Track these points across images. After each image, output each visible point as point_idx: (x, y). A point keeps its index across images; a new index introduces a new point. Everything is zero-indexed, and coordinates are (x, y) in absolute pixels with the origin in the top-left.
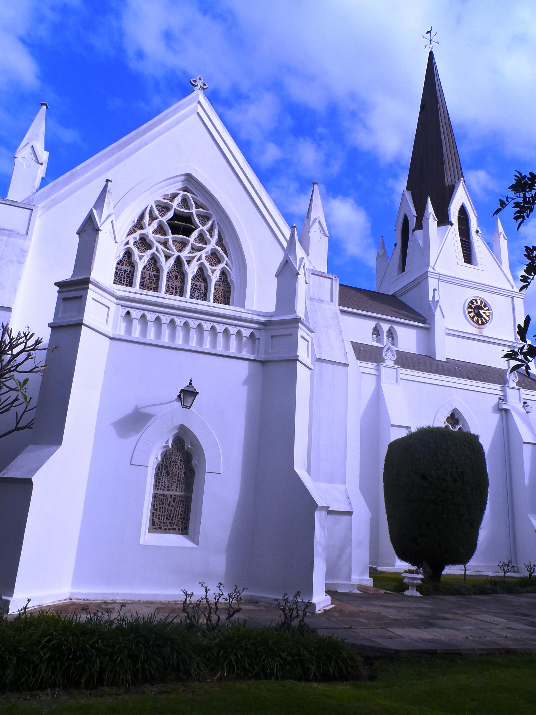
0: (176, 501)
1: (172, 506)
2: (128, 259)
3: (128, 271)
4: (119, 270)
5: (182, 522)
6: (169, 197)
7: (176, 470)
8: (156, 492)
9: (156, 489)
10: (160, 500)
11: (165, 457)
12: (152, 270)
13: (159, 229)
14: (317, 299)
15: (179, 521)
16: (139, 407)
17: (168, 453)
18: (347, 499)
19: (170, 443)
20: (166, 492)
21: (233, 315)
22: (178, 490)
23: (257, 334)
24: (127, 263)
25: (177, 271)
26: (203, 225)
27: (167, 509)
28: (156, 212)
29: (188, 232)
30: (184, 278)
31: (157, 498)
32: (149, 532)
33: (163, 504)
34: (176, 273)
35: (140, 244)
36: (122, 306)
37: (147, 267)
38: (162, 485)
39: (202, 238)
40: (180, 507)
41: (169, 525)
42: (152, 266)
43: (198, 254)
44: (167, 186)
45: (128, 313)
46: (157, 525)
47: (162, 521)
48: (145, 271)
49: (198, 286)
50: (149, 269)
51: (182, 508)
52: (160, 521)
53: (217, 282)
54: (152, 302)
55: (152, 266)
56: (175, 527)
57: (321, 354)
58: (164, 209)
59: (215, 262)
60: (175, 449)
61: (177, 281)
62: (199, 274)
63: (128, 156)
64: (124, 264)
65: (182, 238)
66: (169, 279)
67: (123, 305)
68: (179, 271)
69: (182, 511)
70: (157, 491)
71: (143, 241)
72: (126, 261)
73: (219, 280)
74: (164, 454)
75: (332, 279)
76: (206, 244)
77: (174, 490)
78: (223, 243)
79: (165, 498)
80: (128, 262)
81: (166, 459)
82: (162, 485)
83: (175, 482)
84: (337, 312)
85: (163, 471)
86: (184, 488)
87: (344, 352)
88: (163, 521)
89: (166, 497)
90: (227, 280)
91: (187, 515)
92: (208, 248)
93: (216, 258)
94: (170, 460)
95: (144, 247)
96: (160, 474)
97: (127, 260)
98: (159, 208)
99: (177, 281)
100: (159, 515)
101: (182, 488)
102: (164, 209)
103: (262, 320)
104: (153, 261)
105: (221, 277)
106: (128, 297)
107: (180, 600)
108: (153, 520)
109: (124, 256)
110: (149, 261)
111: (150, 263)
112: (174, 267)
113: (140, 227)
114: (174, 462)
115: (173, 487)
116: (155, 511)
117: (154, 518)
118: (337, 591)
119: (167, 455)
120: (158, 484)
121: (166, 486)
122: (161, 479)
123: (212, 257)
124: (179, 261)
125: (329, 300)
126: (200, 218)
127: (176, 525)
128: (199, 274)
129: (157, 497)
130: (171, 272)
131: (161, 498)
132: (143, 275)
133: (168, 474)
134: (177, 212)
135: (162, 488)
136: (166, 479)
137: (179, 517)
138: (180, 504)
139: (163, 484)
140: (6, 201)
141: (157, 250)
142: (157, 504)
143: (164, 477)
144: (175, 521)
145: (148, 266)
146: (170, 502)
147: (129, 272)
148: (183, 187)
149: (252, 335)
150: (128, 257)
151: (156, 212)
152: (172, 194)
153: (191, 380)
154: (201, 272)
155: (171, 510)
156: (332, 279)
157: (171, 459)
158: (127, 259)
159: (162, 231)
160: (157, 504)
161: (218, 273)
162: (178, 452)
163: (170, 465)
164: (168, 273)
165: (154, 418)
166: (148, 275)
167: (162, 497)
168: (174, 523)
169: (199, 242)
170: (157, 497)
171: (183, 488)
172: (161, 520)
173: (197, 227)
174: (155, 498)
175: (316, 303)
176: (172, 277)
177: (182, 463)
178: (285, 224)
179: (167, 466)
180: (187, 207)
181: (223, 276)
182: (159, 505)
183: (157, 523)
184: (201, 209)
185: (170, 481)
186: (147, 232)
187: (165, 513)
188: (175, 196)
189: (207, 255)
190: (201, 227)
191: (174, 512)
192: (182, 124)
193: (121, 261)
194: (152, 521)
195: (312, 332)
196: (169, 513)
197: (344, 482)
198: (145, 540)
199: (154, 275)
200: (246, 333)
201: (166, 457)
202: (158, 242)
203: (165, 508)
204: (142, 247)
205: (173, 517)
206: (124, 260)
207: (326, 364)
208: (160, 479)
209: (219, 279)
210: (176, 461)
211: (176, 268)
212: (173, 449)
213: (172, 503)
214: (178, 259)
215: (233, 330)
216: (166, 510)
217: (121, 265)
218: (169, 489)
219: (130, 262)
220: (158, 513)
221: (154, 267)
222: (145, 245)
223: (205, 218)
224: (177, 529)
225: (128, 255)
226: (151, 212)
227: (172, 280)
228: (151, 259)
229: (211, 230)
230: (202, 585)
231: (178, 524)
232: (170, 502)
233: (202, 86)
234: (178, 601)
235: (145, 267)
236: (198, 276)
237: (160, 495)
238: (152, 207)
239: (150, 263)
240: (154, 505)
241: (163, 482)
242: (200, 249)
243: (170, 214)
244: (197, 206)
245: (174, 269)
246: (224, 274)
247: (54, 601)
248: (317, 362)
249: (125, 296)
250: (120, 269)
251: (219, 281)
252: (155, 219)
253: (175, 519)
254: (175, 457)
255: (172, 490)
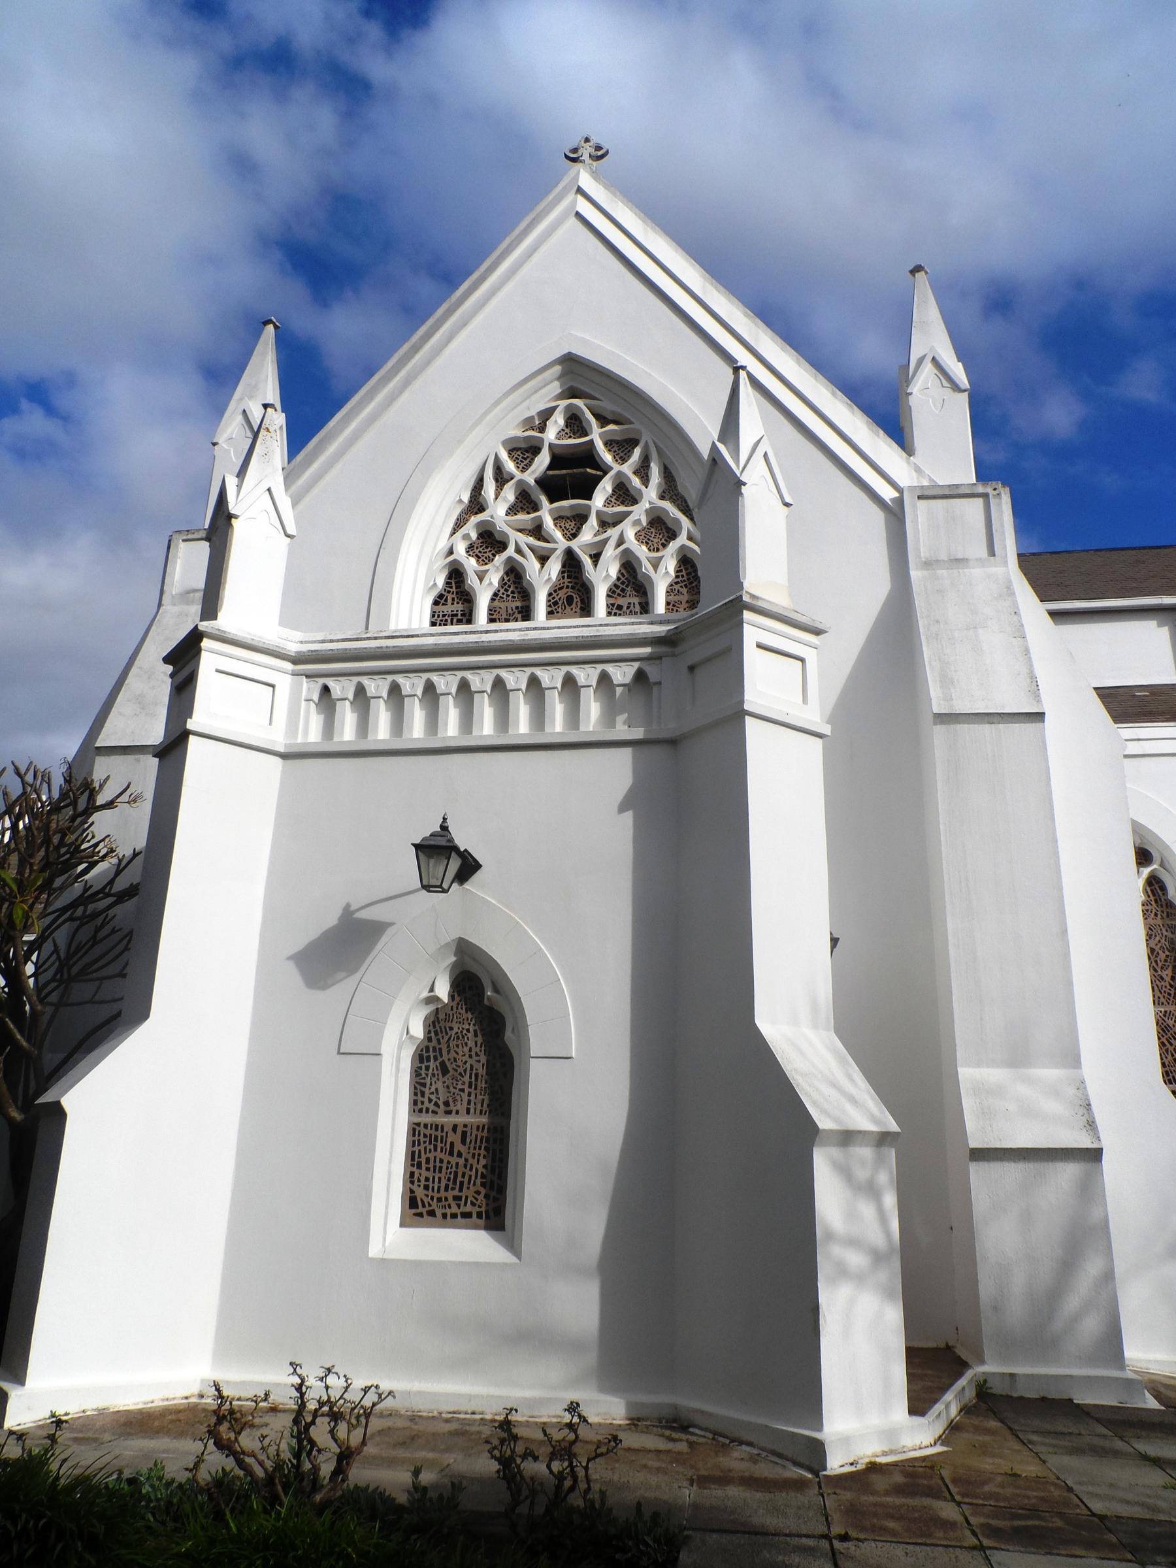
0: (468, 1141)
1: (460, 1155)
2: (456, 588)
3: (459, 613)
4: (439, 616)
5: (486, 1196)
6: (537, 423)
7: (464, 1059)
8: (417, 1120)
9: (417, 1111)
10: (428, 1139)
11: (434, 1027)
12: (513, 597)
13: (521, 502)
14: (946, 559)
15: (478, 1193)
16: (353, 908)
17: (442, 1016)
18: (1082, 1111)
19: (443, 991)
20: (442, 1119)
21: (576, 637)
22: (472, 1111)
23: (653, 672)
24: (454, 596)
25: (570, 585)
26: (623, 460)
27: (445, 1162)
28: (510, 466)
29: (586, 490)
30: (588, 598)
31: (419, 1135)
32: (403, 1224)
33: (435, 1150)
34: (569, 590)
35: (481, 546)
36: (307, 676)
37: (500, 594)
38: (430, 1100)
39: (624, 494)
40: (479, 1155)
41: (453, 1205)
42: (510, 590)
43: (613, 533)
44: (523, 401)
45: (326, 689)
46: (424, 1206)
47: (436, 1195)
48: (496, 603)
49: (625, 608)
50: (505, 596)
51: (484, 1157)
52: (430, 1193)
53: (672, 585)
54: (372, 651)
55: (510, 590)
56: (469, 1208)
57: (952, 699)
58: (528, 452)
59: (663, 541)
60: (458, 1004)
61: (572, 609)
62: (623, 579)
63: (428, 362)
64: (450, 601)
65: (572, 507)
66: (553, 608)
67: (308, 673)
68: (575, 583)
69: (485, 1167)
70: (420, 1117)
71: (488, 539)
72: (453, 593)
73: (676, 580)
74: (432, 1019)
75: (985, 496)
76: (635, 501)
77: (463, 1111)
78: (677, 490)
79: (439, 1133)
80: (457, 593)
81: (436, 1033)
82: (430, 1100)
83: (462, 1090)
84: (1010, 582)
85: (432, 1065)
86: (488, 1106)
87: (1028, 681)
88: (439, 1195)
89: (442, 1130)
90: (697, 575)
91: (500, 1177)
92: (639, 513)
93: (664, 531)
94: (447, 1034)
95: (490, 551)
96: (423, 1072)
97: (454, 589)
98: (516, 456)
99: (572, 609)
100: (427, 1179)
101: (482, 1106)
102: (527, 455)
103: (660, 632)
104: (512, 577)
105: (681, 571)
106: (315, 651)
107: (470, 1411)
108: (412, 1191)
109: (447, 583)
110: (504, 580)
111: (505, 584)
112: (563, 577)
113: (479, 509)
114: (458, 1037)
115: (459, 1103)
116: (415, 1169)
117: (415, 1188)
118: (1071, 1400)
119: (439, 1023)
120: (419, 1098)
121: (440, 1103)
122: (428, 1085)
123: (652, 530)
124: (571, 563)
125: (983, 552)
126: (616, 448)
127: (473, 1204)
128: (623, 579)
129: (419, 1131)
130: (555, 591)
131: (431, 1135)
132: (493, 615)
133: (444, 1070)
134: (557, 451)
135: (432, 1107)
136: (440, 1085)
137: (479, 1181)
138: (480, 1148)
139: (433, 1097)
140: (193, 533)
141: (519, 551)
142: (420, 1151)
143: (434, 1079)
144: (469, 1192)
145: (502, 591)
146: (452, 1144)
147: (462, 615)
148: (566, 390)
149: (640, 676)
150: (456, 583)
151: (510, 466)
152: (540, 413)
153: (445, 819)
154: (628, 572)
155: (457, 1164)
156: (985, 496)
157: (450, 1033)
158: (454, 587)
159: (527, 504)
160: (420, 1151)
161: (670, 565)
162: (467, 1012)
163: (448, 1046)
164: (550, 595)
165: (390, 932)
166: (503, 612)
167: (433, 1132)
168: (467, 1197)
169: (618, 503)
170: (419, 1131)
171: (485, 1105)
172: (433, 1191)
173: (605, 470)
174: (414, 1135)
175: (942, 572)
176: (560, 603)
177: (480, 1039)
178: (834, 394)
179: (440, 1049)
180: (580, 432)
181: (686, 569)
182: (426, 1153)
183: (421, 1200)
184: (612, 427)
185: (452, 1090)
186: (492, 517)
187: (440, 1171)
188: (547, 414)
189: (639, 528)
190: (617, 468)
191: (464, 1170)
192: (543, 250)
193: (441, 596)
194: (409, 1194)
195: (817, 632)
196: (451, 1173)
197: (1074, 1060)
198: (387, 1244)
199: (517, 608)
200: (622, 674)
201: (438, 1028)
202: (520, 531)
203: (441, 1161)
204: (486, 552)
205: (462, 1183)
206: (449, 592)
207: (971, 726)
208: (424, 1085)
209: (677, 577)
210: (463, 1037)
211: (566, 580)
212: (454, 1004)
213: (458, 1147)
214: (569, 553)
215: (586, 676)
216: (445, 1165)
217: (443, 604)
218: (448, 1109)
219: (461, 592)
220: (424, 1173)
221: (516, 591)
222: (493, 547)
223: (621, 447)
224: (474, 1215)
225: (455, 579)
226: (499, 469)
227: (560, 610)
228: (507, 573)
229: (643, 472)
230: (295, 1370)
231: (477, 1200)
232: (452, 1144)
233: (594, 153)
234: (466, 1413)
235: (495, 595)
236: (623, 583)
237: (426, 1126)
238: (497, 458)
239: (505, 584)
240: (413, 1153)
241: (432, 1093)
242: (619, 519)
243: (543, 460)
244: (603, 420)
245: (564, 583)
246: (686, 562)
247: (150, 1399)
248: (938, 726)
249: (309, 651)
250: (441, 614)
251: (677, 583)
252: (508, 481)
253: (468, 1188)
254: (461, 1026)
255: (457, 1112)
